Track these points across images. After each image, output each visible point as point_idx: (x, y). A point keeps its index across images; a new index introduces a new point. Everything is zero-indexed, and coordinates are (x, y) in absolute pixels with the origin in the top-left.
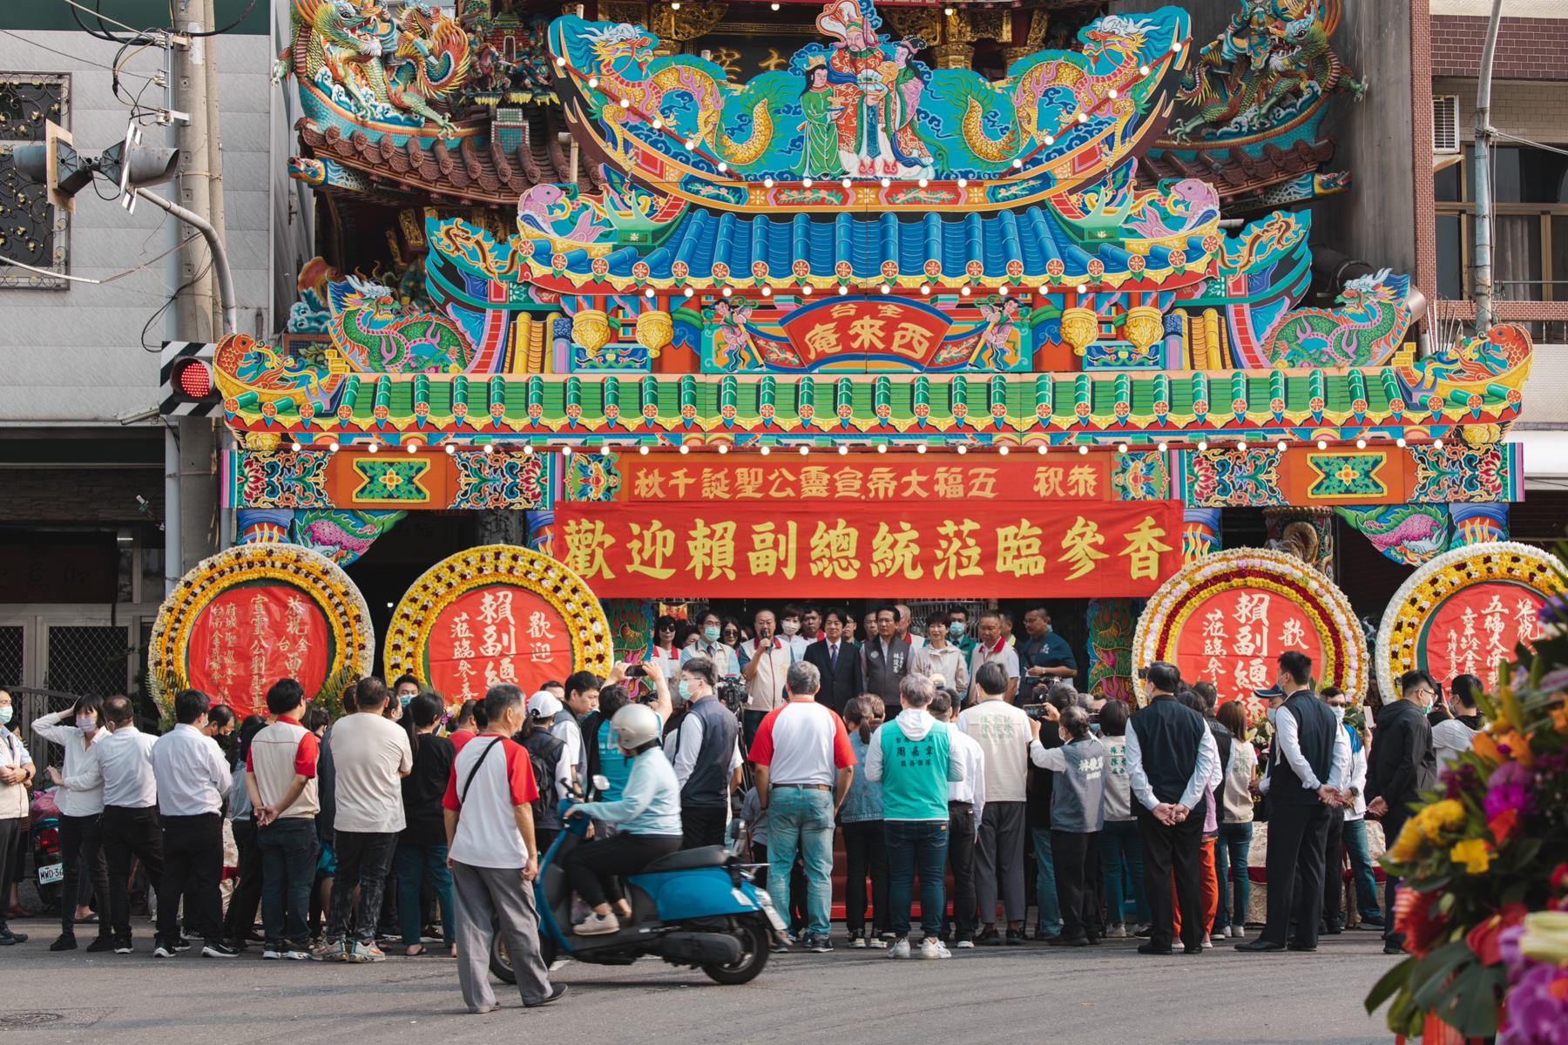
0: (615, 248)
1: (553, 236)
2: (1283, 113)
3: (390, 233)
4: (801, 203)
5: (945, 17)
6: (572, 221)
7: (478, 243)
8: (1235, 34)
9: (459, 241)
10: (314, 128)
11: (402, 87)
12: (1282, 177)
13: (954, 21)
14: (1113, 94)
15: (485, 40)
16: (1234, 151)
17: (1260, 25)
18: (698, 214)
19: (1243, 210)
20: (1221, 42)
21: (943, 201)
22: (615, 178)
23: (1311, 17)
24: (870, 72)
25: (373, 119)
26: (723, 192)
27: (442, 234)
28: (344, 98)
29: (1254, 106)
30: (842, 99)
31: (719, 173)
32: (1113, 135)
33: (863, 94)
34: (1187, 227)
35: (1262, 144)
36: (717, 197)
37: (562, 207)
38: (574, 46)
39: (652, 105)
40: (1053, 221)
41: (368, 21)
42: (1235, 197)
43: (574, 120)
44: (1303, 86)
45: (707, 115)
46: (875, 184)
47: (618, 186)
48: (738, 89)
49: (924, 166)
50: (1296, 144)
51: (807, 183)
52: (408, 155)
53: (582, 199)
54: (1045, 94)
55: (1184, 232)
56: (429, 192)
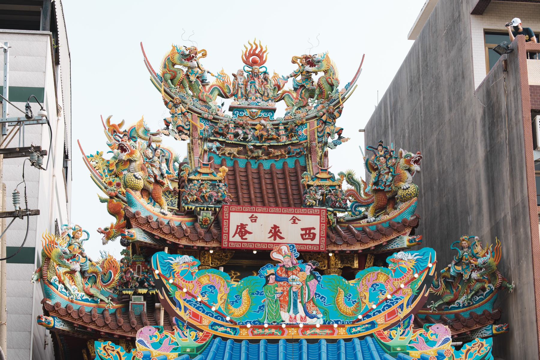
0: (180, 355)
1: (152, 349)
2: (478, 298)
3: (84, 351)
4: (263, 335)
5: (329, 257)
6: (160, 343)
7: (118, 352)
8: (456, 264)
9: (109, 352)
10: (50, 303)
11: (90, 286)
12: (478, 326)
13: (333, 259)
14: (402, 286)
15: (128, 266)
16: (457, 315)
17: (466, 260)
18: (217, 340)
19: (462, 338)
20: (450, 268)
21: (327, 334)
22: (180, 324)
23: (489, 256)
24: (294, 276)
25: (77, 299)
26: (228, 330)
27: (102, 349)
28: (64, 290)
29: (465, 296)
30: (282, 288)
31: (227, 321)
32: (403, 304)
33: (291, 286)
34: (437, 345)
35: (469, 312)
36: (226, 332)
37: (156, 337)
38: (163, 265)
39: (197, 291)
40: (377, 342)
41: (74, 256)
42: (457, 335)
43: (162, 298)
44: (486, 286)
45: (221, 295)
46: (297, 326)
47: (181, 327)
48: (235, 284)
49: (318, 318)
50: (484, 312)
51: (266, 326)
52: (91, 315)
53: (165, 333)
54: (372, 286)
55: (435, 348)
56: (100, 332)
